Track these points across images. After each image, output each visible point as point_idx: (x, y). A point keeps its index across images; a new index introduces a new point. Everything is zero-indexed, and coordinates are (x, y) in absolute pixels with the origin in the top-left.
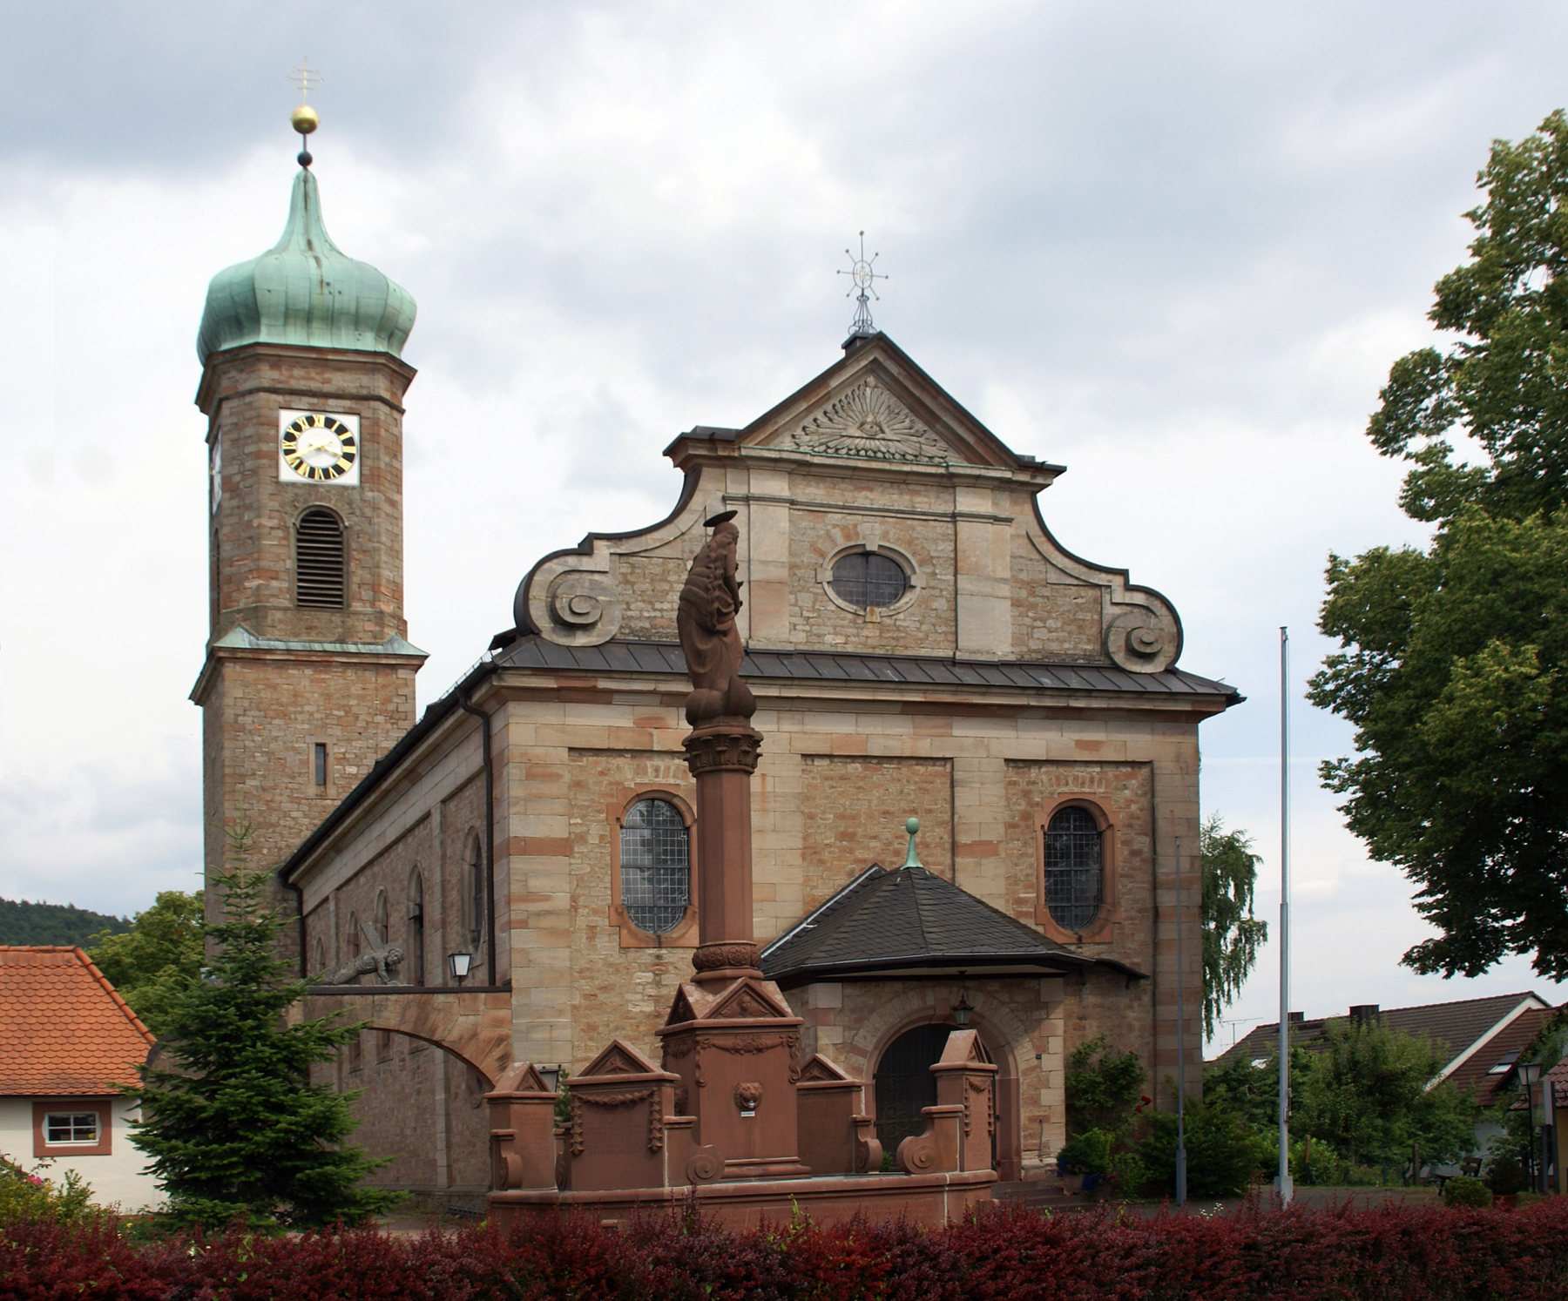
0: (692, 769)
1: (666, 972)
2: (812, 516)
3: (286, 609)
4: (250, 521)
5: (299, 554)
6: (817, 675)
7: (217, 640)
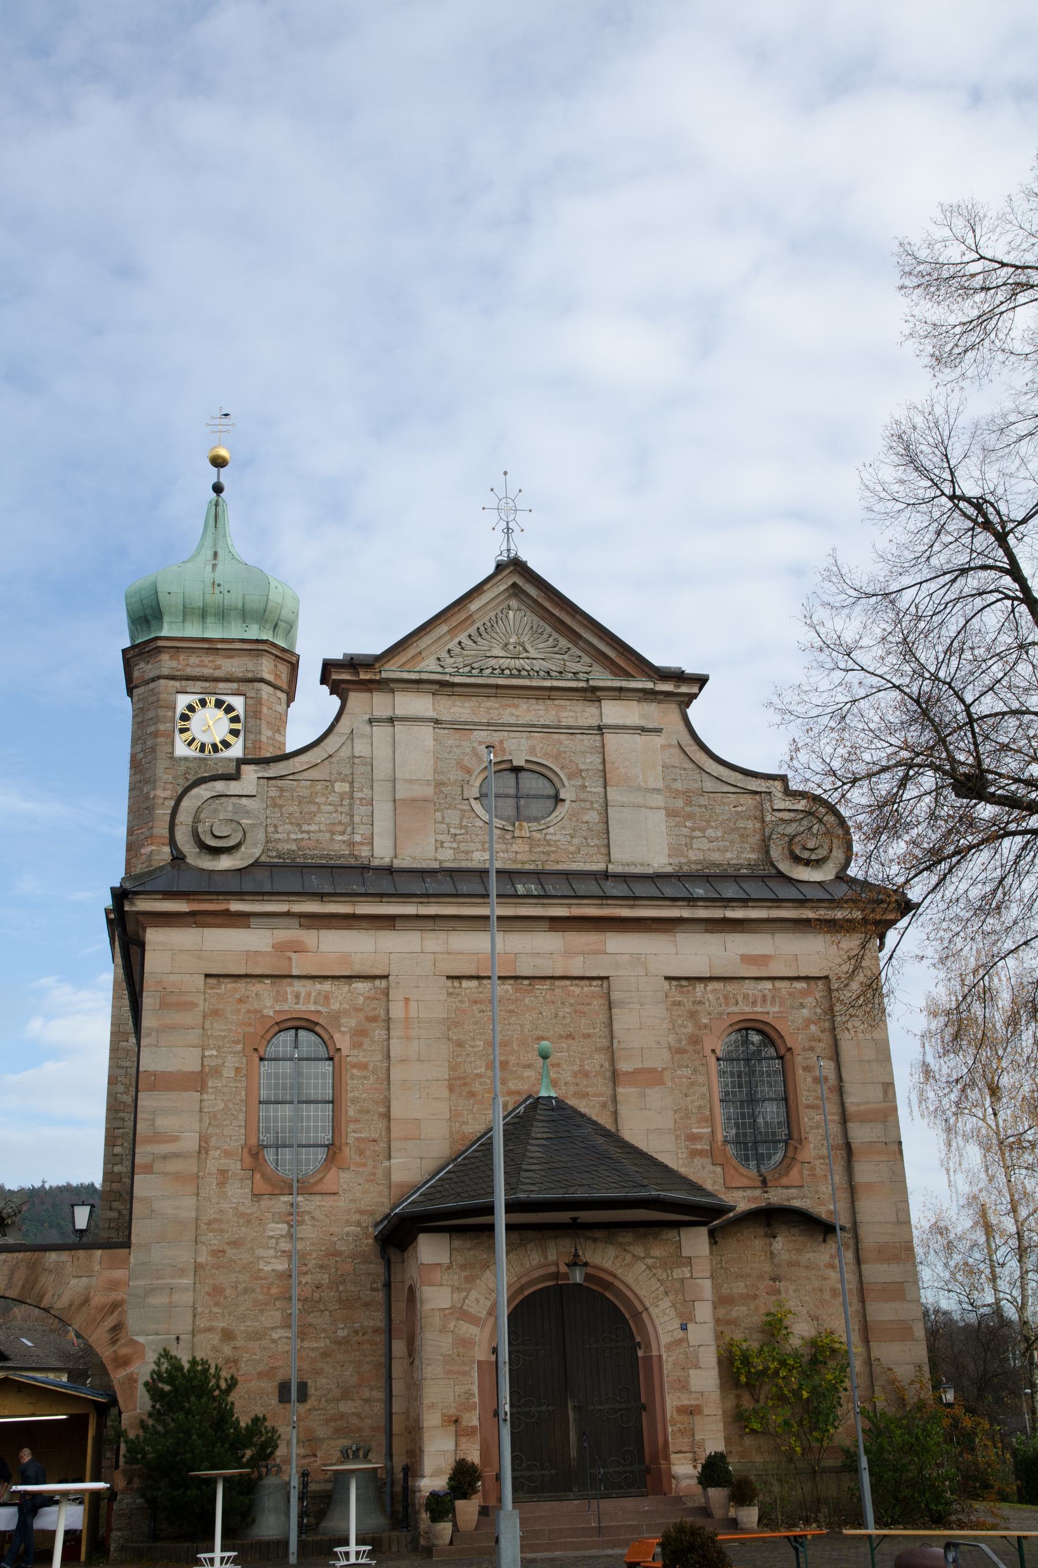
1: (301, 1223)
2: (458, 734)
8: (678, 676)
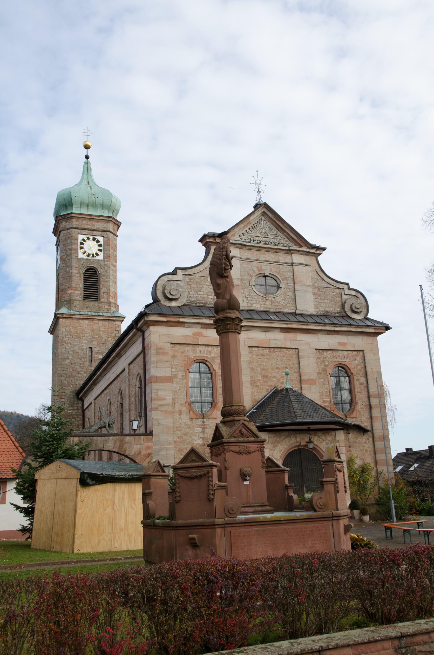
0: (217, 332)
1: (206, 428)
2: (247, 263)
3: (80, 301)
4: (69, 271)
5: (84, 282)
6: (251, 318)
7: (58, 310)
8: (318, 248)
